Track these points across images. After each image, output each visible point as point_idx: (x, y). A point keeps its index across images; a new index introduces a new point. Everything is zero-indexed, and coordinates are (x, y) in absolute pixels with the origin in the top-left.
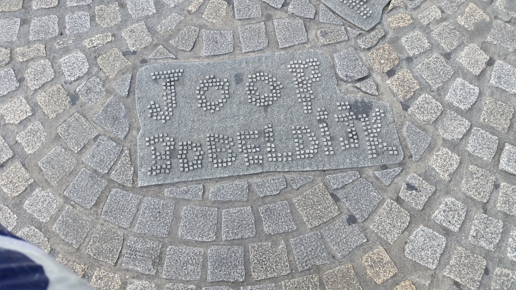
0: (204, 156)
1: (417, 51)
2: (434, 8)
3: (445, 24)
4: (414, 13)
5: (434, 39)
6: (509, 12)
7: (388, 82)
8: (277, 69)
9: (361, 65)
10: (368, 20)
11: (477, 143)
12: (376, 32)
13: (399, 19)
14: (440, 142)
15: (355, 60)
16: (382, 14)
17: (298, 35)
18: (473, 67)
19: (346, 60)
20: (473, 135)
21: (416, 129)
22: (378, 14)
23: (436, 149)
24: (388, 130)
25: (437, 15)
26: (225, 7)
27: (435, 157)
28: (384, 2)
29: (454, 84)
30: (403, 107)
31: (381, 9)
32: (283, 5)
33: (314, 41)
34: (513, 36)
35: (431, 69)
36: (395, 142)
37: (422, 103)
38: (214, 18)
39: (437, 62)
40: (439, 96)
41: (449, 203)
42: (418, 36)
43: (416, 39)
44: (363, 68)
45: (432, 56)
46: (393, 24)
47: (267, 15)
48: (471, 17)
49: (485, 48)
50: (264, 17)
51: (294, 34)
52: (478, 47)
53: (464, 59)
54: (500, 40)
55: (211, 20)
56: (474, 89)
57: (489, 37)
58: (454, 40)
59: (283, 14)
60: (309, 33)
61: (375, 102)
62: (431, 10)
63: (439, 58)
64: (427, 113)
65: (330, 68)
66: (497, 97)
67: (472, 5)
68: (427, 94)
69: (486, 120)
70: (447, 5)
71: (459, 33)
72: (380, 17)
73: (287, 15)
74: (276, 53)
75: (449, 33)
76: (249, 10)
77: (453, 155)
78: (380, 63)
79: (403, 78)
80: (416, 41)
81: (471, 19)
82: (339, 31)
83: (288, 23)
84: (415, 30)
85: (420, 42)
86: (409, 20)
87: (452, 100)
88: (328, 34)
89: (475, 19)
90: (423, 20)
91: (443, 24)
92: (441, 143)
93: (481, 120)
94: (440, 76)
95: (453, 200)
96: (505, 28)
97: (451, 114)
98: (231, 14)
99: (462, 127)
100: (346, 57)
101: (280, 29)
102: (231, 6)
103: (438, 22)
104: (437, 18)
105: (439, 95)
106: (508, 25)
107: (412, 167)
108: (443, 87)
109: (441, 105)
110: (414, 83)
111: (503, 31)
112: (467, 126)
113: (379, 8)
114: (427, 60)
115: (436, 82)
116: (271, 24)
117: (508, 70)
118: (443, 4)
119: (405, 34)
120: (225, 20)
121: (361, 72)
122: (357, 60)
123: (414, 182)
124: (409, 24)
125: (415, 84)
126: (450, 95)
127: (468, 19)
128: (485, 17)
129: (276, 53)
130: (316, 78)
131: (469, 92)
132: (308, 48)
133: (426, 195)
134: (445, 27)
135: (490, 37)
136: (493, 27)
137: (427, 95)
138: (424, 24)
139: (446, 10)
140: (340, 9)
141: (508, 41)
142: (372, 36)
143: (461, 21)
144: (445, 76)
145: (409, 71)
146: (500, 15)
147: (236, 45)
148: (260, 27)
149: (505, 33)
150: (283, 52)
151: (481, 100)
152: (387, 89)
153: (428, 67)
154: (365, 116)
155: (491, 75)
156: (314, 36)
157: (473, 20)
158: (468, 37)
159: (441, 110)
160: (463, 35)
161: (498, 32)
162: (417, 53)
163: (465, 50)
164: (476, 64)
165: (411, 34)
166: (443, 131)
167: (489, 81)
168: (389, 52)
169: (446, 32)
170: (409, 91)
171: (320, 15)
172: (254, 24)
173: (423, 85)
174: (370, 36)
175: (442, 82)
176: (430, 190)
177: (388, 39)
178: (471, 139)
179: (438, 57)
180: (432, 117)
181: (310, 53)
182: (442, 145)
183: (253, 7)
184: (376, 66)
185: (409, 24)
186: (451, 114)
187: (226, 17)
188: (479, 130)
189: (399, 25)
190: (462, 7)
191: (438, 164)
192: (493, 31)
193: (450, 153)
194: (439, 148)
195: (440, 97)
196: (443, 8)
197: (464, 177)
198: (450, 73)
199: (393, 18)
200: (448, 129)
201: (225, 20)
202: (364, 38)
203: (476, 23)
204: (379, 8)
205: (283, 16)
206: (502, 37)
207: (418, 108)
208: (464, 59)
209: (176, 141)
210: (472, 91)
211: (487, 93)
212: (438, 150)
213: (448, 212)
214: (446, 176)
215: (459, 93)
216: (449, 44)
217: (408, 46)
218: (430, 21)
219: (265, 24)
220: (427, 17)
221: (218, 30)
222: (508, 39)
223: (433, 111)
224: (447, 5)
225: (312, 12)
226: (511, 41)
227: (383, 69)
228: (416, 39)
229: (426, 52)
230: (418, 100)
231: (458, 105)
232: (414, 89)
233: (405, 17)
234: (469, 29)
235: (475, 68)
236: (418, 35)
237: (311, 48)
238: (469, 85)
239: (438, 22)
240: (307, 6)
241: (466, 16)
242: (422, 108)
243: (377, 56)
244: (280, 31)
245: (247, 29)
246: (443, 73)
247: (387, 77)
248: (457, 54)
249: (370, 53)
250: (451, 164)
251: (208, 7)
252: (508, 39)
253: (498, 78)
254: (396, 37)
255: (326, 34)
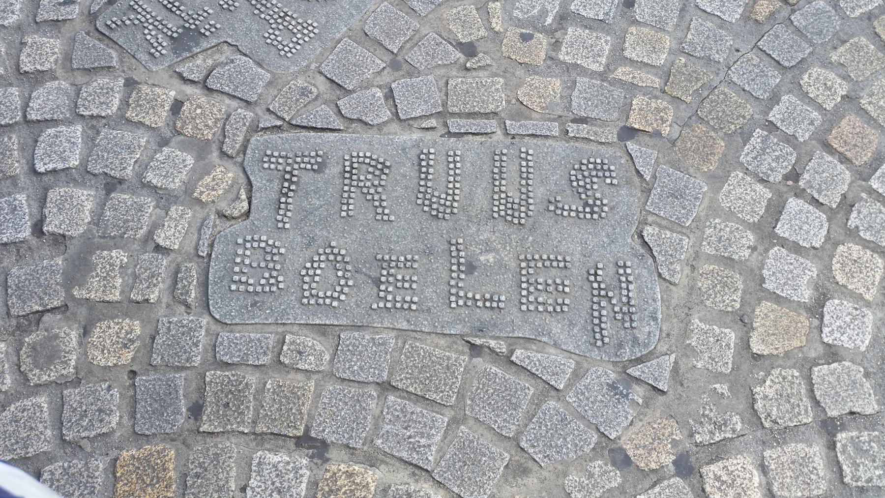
0: (395, 126)
1: (160, 159)
2: (175, 244)
3: (142, 231)
4: (200, 215)
5: (145, 196)
6: (46, 334)
7: (173, 93)
8: (327, 13)
9: (224, 87)
10: (262, 153)
11: (6, 103)
12: (236, 143)
13: (217, 184)
14: (59, 72)
15: (238, 87)
16: (248, 178)
17: (338, 67)
18: (62, 196)
19: (248, 80)
20: (16, 108)
21: (100, 64)
22: (253, 172)
23: (60, 62)
24: (135, 41)
25: (163, 235)
26: (460, 36)
27: (56, 50)
28: (258, 195)
29: (77, 152)
30: (133, 80)
31: (254, 183)
32: (391, 90)
33: (311, 77)
34: (20, 296)
35: (123, 149)
36: (118, 34)
37: (110, 99)
38: (459, 14)
39: (121, 164)
40: (93, 126)
41: (10, 15)
42: (171, 180)
43: (172, 174)
44: (219, 85)
45: (134, 168)
46: (222, 172)
47: (401, 66)
48: (105, 275)
49: (60, 240)
50: (402, 61)
51: (344, 65)
52: (70, 233)
53: (83, 198)
54: (40, 272)
55: (460, 8)
56: (45, 164)
57: (60, 263)
58: (113, 218)
59: (381, 81)
60: (328, 82)
61: (173, 60)
62: (177, 235)
63: (121, 170)
64: (96, 92)
65: (263, 60)
66: (5, 183)
67: (115, 296)
68: (111, 114)
69: (6, 139)
70: (157, 266)
71: (112, 234)
72: (248, 169)
73: (375, 84)
74: (346, 29)
75: (127, 221)
76: (427, 53)
77: (32, 68)
78: (201, 108)
79: (156, 110)
80: (171, 171)
81: (104, 270)
82: (290, 109)
83: (364, 73)
84: (183, 188)
85: (163, 174)
86: (202, 193)
87: (69, 130)
88: (300, 96)
89: (97, 275)
90: (180, 211)
91: (145, 228)
92: (58, 74)
93: (14, 137)
94: (106, 150)
95: (7, 21)
96: (41, 299)
97: (62, 113)
98: (444, 34)
99: (38, 107)
100: (252, 82)
101: (367, 59)
102: (454, 44)
103: (155, 226)
104: (159, 231)
105: (93, 127)
106: (37, 308)
107: (80, 26)
108: (93, 140)
109: (82, 113)
110: (137, 116)
111: (42, 291)
112: (32, 112)
113: (258, 182)
114: (138, 156)
115: (107, 138)
116: (385, 59)
117: (5, 231)
118: (164, 263)
119: (193, 170)
120: (445, 22)
121: (217, 78)
122: (234, 90)
123: (67, 9)
124: (196, 188)
125: (134, 115)
126: (76, 133)
127: (108, 266)
128: (84, 292)
129: (346, 29)
130: (328, 254)
131: (50, 156)
132: (311, 63)
133: (45, 5)
134: (139, 226)
135: (57, 264)
136: (61, 286)
137: (109, 111)
138: (175, 207)
139: (153, 257)
140: (312, 140)
141: (26, 279)
142: (239, 133)
143: (119, 256)
144: (98, 155)
145: (153, 125)
146: (60, 319)
147: (401, 4)
148: (394, 43)
149: (36, 290)
150: (338, 36)
151: (27, 164)
152: (168, 86)
153: (129, 148)
154: (175, 35)
155: (29, 206)
156: (318, 84)
157: (99, 271)
158: (94, 238)
159: (79, 108)
160: (104, 237)
161: (49, 281)
162: (158, 156)
163: (87, 213)
164: (60, 204)
165: (184, 176)
166: (62, 86)
167: (28, 196)
168: (199, 129)
169: (133, 220)
170: (138, 101)
171: (331, 113)
172: (405, 43)
173: (124, 124)
174: (240, 131)
175: (98, 145)
176: (42, 15)
177: (213, 150)
178: (18, 102)
179: (123, 171)
180: (86, 92)
181: (304, 59)
182: (55, 72)
183: (426, 61)
184: (203, 99)
185: (196, 188)
186: (62, 113)
187: (447, 26)
188: (11, 119)
189: (212, 176)
190: (131, 281)
191: (48, 45)
192: (59, 278)
193: (39, 67)
194: (56, 65)
195: (90, 124)
196: (160, 257)
197: (5, 57)
198: (93, 164)
199: (226, 179)
200: (56, 94)
201: (445, 22)
202: (247, 124)
203: (92, 271)
204: (258, 182)
205: (378, 79)
206: (38, 279)
207: (112, 89)
208: (83, 198)
209: (497, 310)
210: (47, 160)
211: (22, 179)
212: (56, 61)
213: (6, 7)
214: (30, 40)
215: (65, 144)
216: (118, 205)
217: (177, 156)
218: (168, 218)
219: (392, 53)
220: (176, 220)
221: (439, 5)
222: (27, 282)
223: (89, 99)
224: (157, 266)
225: (347, 108)
226: (20, 285)
227: (191, 103)
228: (172, 174)
229: (143, 166)
230: (117, 99)
231: (59, 129)
232: (132, 108)
233: (209, 194)
234: (98, 252)
235: (59, 197)
236: (173, 181)
237: (308, 66)
238: (55, 166)
239: (155, 226)
240: (360, 111)
241: (114, 269)
242: (107, 93)
243: (211, 113)
244: (364, 56)
245: (407, 31)
246: (103, 156)
247: (179, 98)
248: (98, 200)
249: (223, 110)
250: (30, 55)
251: (479, 20)
252: (27, 282)
253: (16, 207)
254: (203, 159)
255: (303, 94)
